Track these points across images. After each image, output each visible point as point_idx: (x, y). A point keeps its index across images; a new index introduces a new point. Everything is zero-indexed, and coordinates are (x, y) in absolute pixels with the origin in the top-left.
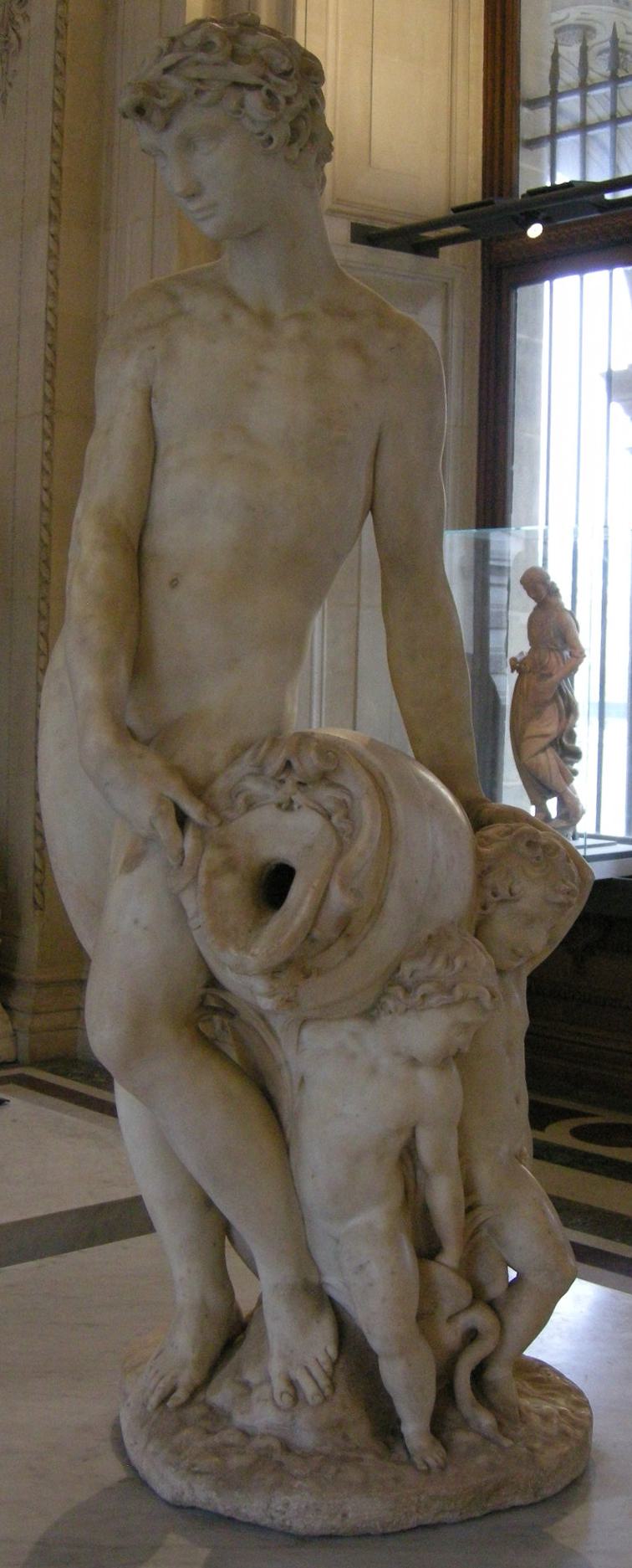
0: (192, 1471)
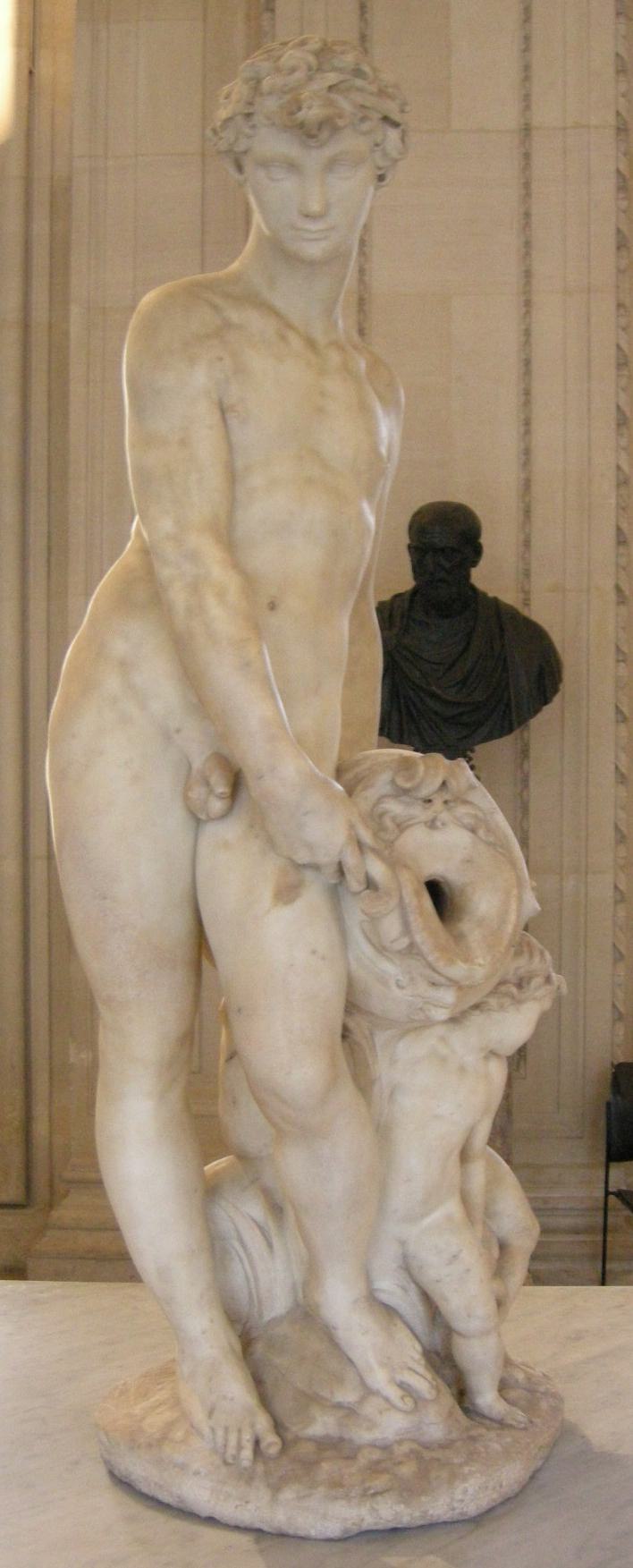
0: (369, 1495)
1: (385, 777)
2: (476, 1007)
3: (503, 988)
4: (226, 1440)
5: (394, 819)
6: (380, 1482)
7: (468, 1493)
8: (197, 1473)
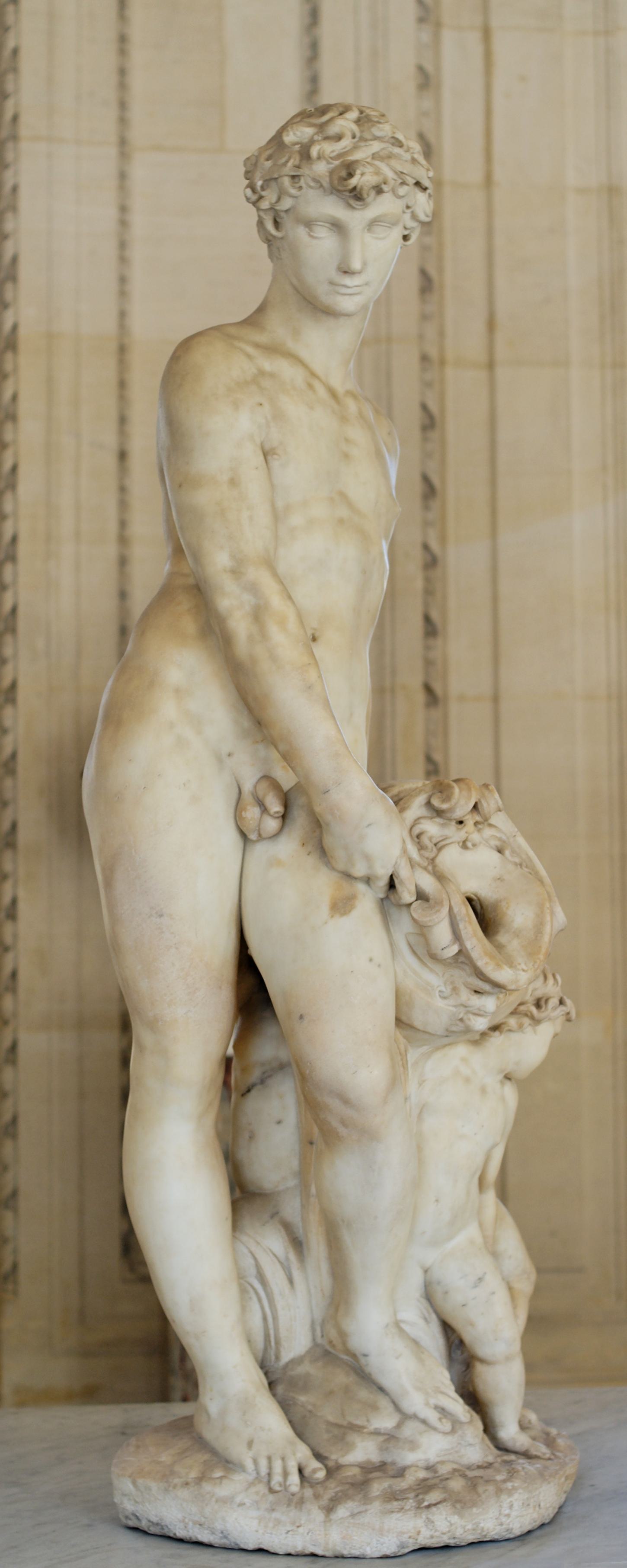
1: (421, 799)
2: (495, 1028)
3: (522, 1008)
4: (270, 1468)
5: (430, 839)
6: (434, 1496)
7: (512, 1509)
8: (242, 1504)
